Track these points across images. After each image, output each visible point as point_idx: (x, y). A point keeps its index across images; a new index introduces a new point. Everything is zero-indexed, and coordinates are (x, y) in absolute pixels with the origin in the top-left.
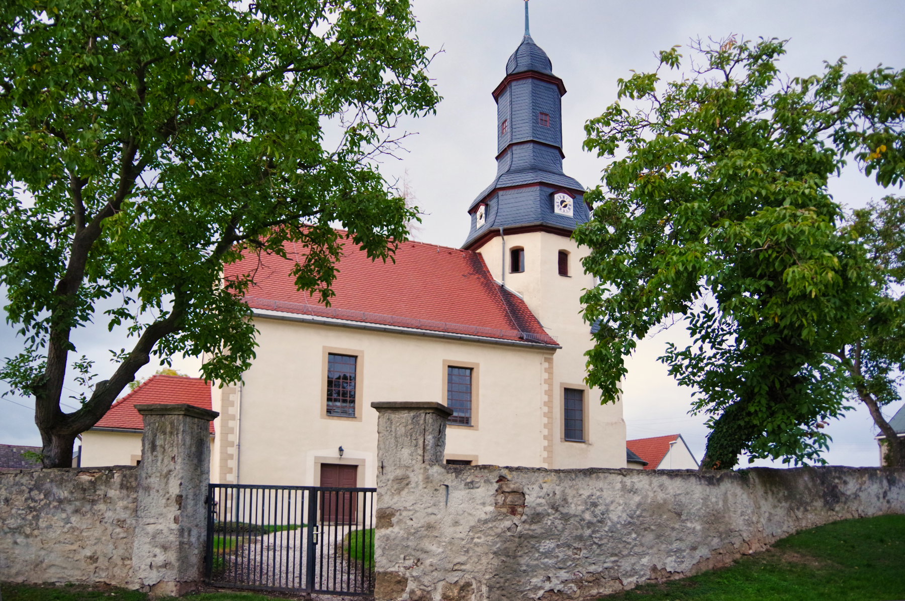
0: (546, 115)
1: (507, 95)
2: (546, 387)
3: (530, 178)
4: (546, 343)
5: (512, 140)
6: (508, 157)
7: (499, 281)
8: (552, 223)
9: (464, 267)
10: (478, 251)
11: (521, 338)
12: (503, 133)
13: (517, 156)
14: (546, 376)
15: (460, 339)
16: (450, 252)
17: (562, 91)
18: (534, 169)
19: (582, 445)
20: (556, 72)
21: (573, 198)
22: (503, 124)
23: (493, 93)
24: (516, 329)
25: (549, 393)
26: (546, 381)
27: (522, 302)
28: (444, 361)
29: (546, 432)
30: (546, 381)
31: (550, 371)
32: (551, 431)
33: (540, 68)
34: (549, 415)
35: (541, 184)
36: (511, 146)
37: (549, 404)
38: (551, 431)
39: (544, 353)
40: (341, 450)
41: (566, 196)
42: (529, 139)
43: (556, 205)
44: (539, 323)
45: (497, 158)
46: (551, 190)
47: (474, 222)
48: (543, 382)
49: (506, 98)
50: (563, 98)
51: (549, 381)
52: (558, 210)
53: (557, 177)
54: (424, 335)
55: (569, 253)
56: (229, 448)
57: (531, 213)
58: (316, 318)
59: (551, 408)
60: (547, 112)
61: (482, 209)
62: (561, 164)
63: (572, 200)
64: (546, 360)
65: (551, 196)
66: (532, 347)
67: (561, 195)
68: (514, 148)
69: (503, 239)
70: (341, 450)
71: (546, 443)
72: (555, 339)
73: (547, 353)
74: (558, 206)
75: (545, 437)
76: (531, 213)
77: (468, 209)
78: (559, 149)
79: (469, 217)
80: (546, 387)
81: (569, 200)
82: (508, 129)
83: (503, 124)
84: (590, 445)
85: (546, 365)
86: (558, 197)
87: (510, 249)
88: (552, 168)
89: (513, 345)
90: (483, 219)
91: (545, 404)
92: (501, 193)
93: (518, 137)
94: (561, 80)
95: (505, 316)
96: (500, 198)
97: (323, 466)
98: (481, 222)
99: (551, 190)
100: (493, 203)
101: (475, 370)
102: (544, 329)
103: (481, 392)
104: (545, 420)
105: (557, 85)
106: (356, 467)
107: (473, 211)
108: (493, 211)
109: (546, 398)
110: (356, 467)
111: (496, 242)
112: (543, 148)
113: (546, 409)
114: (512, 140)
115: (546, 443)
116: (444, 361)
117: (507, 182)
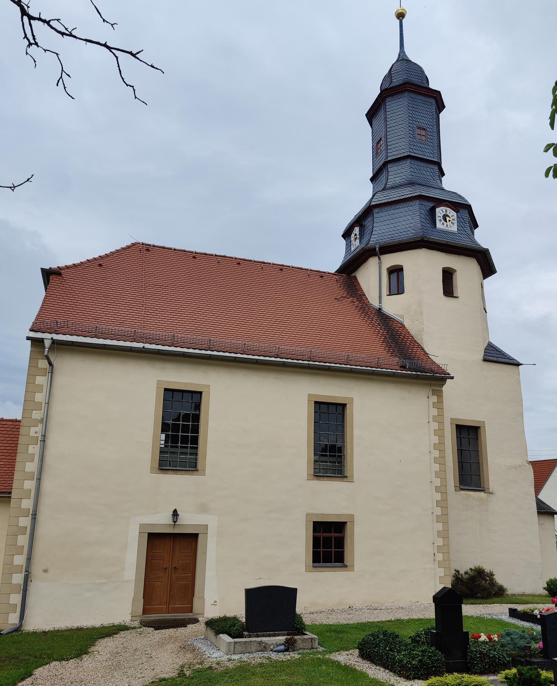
0: (424, 129)
1: (381, 114)
2: (435, 426)
3: (407, 192)
4: (432, 371)
5: (387, 157)
6: (383, 177)
7: (375, 303)
8: (434, 237)
9: (338, 291)
10: (353, 275)
11: (403, 367)
12: (377, 153)
13: (393, 173)
14: (434, 412)
15: (329, 369)
16: (321, 275)
17: (440, 106)
18: (411, 184)
19: (482, 494)
20: (432, 86)
21: (457, 212)
22: (378, 143)
23: (366, 115)
24: (396, 356)
25: (439, 433)
26: (435, 419)
27: (403, 326)
28: (310, 396)
29: (438, 482)
30: (435, 419)
31: (439, 405)
32: (444, 480)
33: (416, 80)
34: (440, 460)
35: (421, 197)
36: (386, 164)
37: (440, 446)
38: (444, 480)
39: (431, 385)
40: (175, 514)
41: (449, 210)
42: (405, 154)
43: (438, 219)
44: (423, 349)
45: (372, 180)
46: (431, 205)
47: (348, 246)
48: (431, 420)
49: (379, 120)
50: (441, 115)
51: (439, 418)
52: (439, 225)
53: (437, 191)
54: (284, 365)
55: (455, 271)
56: (21, 519)
57: (410, 229)
58: (148, 346)
59: (442, 451)
60: (425, 126)
61: (357, 230)
62: (441, 181)
63: (455, 214)
64: (434, 393)
65: (432, 212)
66: (417, 377)
67: (444, 208)
68: (390, 166)
69: (379, 259)
70: (175, 514)
71: (438, 496)
72: (480, 243)
73: (435, 385)
74: (440, 220)
75: (437, 489)
76: (410, 229)
77: (342, 233)
78: (438, 164)
79: (343, 242)
80: (435, 426)
81: (452, 213)
82: (383, 148)
83: (378, 143)
84: (491, 493)
85: (434, 399)
86: (440, 211)
87: (388, 269)
88: (433, 183)
89: (393, 375)
90: (358, 241)
91: (435, 446)
92: (376, 211)
93: (394, 153)
94: (439, 92)
95: (384, 342)
96: (375, 215)
97: (152, 536)
98: (356, 244)
99: (431, 205)
100: (367, 222)
101: (348, 406)
102: (430, 356)
103: (211, 424)
104: (437, 467)
105: (435, 98)
106: (196, 536)
107: (347, 235)
108: (367, 231)
109: (436, 440)
110: (196, 536)
111: (373, 262)
112: (422, 164)
113: (436, 454)
114: (387, 157)
115: (438, 496)
116: (310, 396)
117: (382, 198)
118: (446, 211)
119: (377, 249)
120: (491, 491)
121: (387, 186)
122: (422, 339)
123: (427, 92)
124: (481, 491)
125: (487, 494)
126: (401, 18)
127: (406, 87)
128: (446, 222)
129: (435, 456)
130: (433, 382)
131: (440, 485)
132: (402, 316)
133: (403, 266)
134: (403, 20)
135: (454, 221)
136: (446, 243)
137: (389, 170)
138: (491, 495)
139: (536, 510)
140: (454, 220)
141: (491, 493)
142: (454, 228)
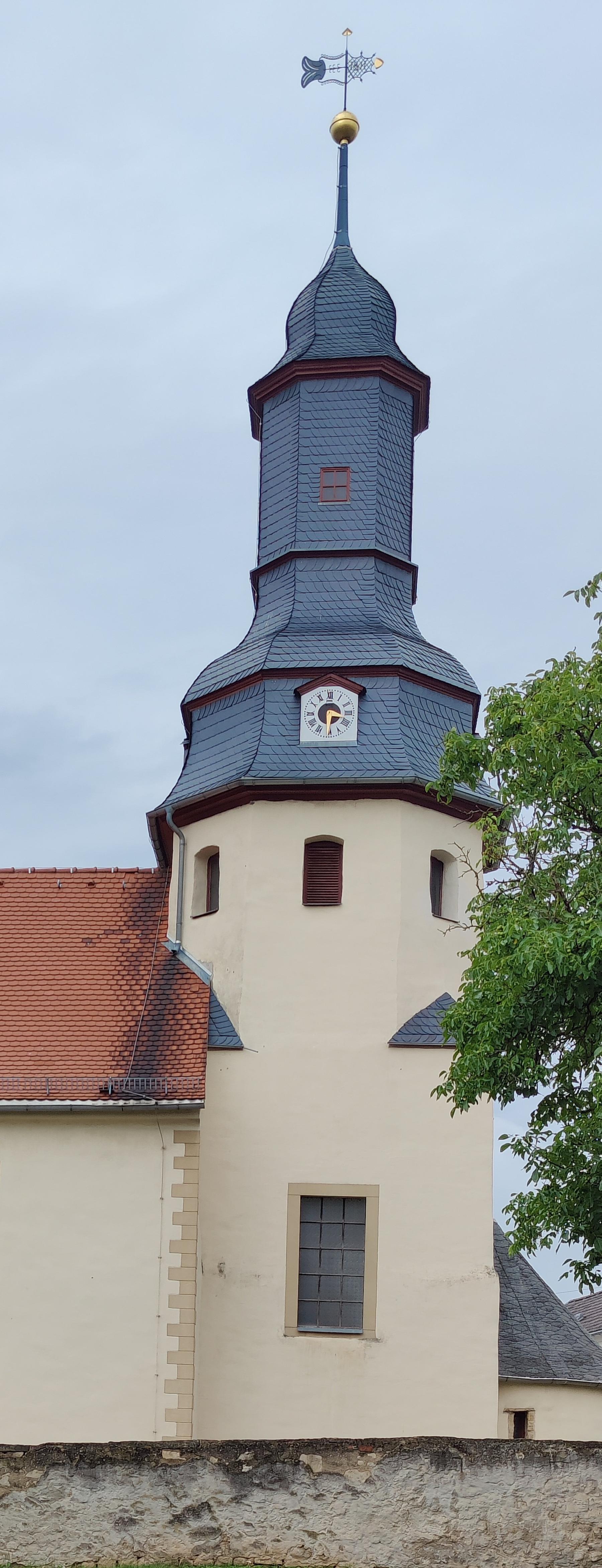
19: (353, 1342)
43: (304, 720)
48: (168, 1192)
60: (342, 461)
74: (312, 723)
84: (377, 1340)
85: (180, 1150)
118: (330, 695)
119: (169, 816)
120: (377, 1337)
121: (289, 626)
122: (237, 1014)
123: (353, 367)
124: (352, 1336)
125: (364, 1342)
126: (343, 142)
127: (293, 372)
128: (325, 721)
129: (172, 1266)
130: (160, 1117)
131: (178, 1322)
132: (210, 965)
133: (218, 848)
134: (350, 146)
135: (348, 718)
136: (302, 783)
137: (299, 576)
138: (374, 1344)
139: (496, 1376)
140: (349, 713)
141: (377, 1340)
142: (349, 734)
